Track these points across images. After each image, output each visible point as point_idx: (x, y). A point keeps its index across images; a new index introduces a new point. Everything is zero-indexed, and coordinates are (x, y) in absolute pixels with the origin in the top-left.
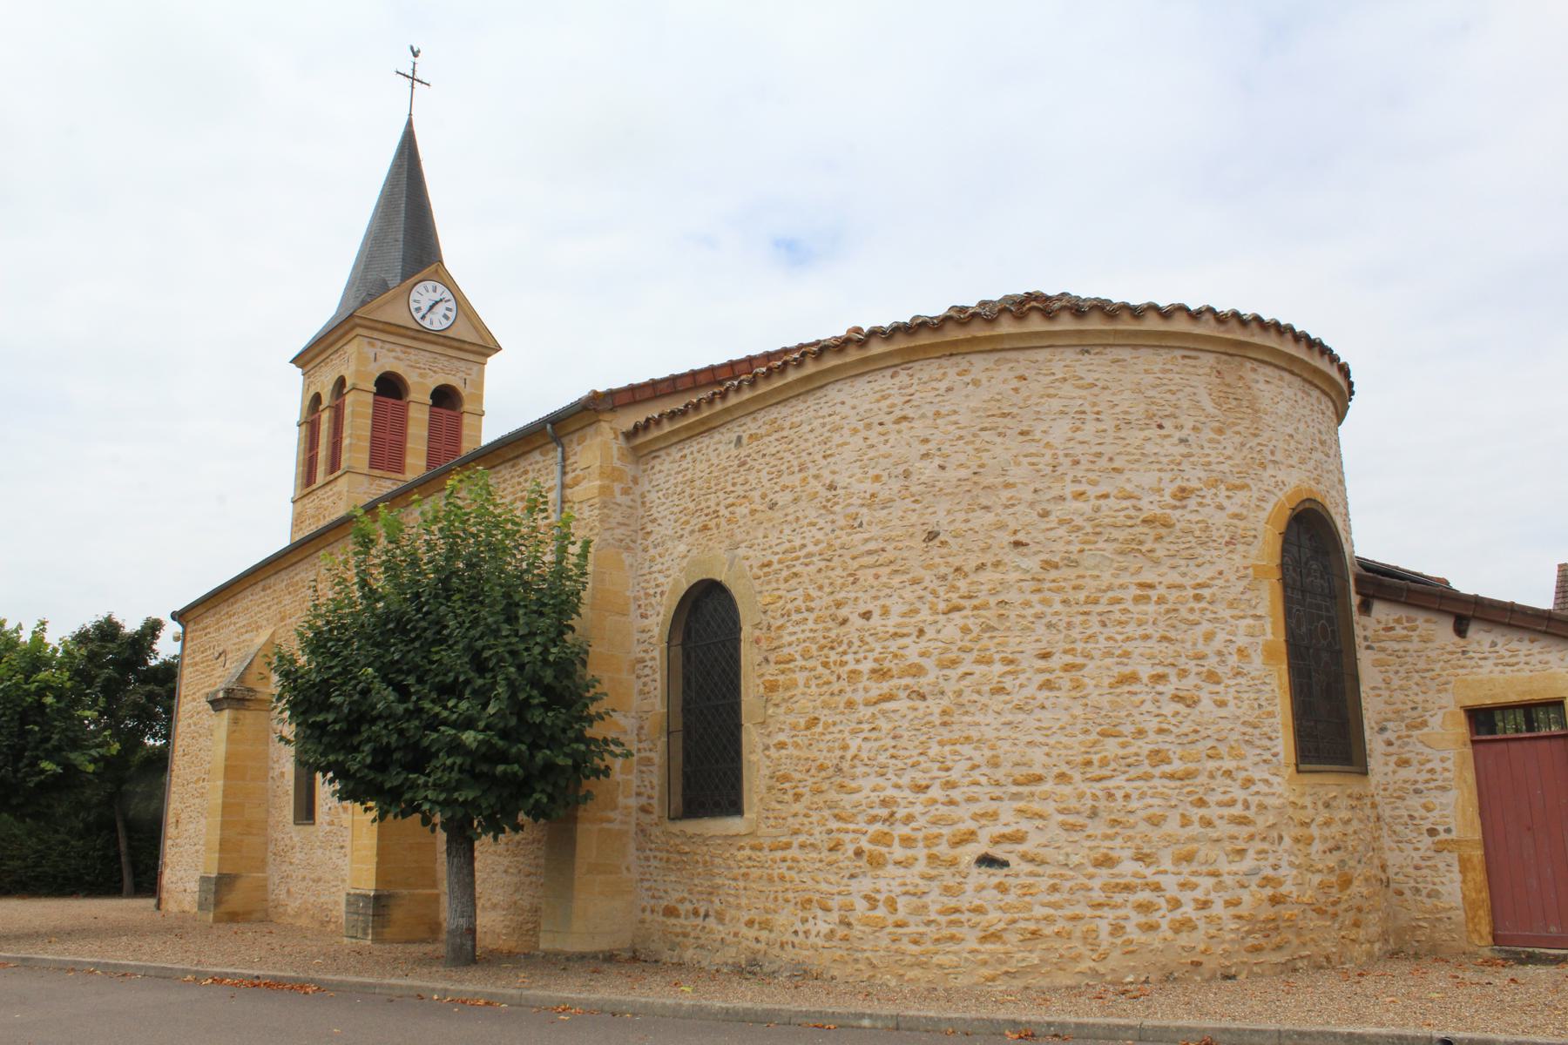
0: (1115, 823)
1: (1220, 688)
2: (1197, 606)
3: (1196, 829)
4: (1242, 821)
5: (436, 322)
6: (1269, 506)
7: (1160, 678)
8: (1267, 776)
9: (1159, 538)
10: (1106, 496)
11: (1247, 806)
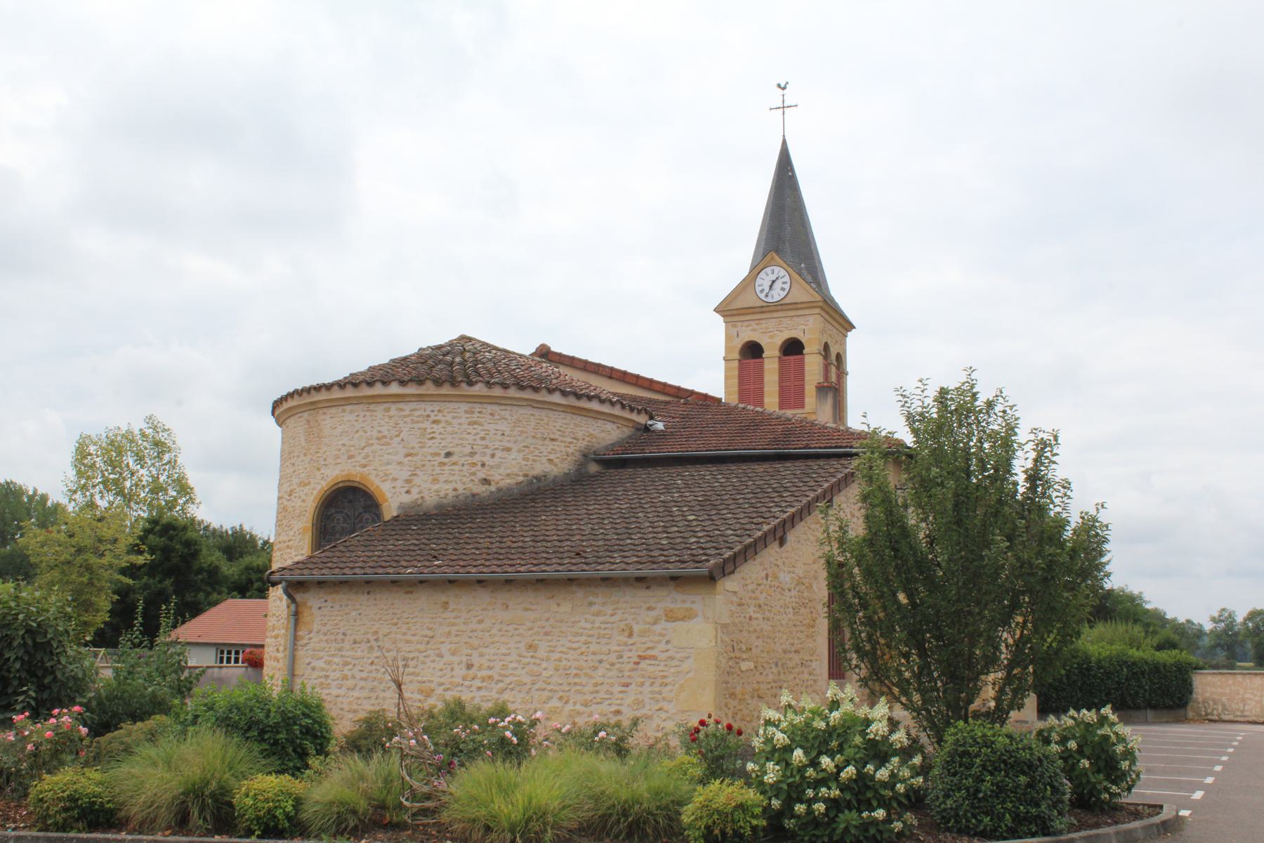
5: (777, 295)
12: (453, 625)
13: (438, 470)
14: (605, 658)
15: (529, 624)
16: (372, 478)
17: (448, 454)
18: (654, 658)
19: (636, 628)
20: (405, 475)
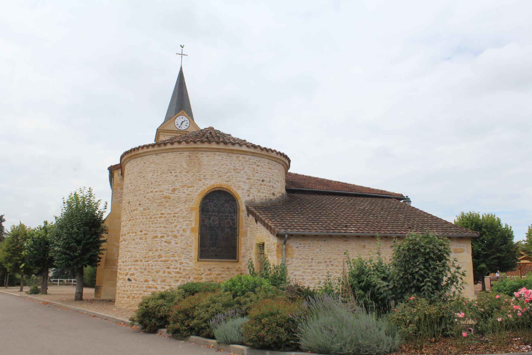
0: (149, 272)
1: (177, 239)
2: (174, 218)
3: (166, 274)
4: (178, 273)
6: (199, 191)
7: (162, 237)
8: (188, 262)
9: (167, 202)
10: (156, 192)
11: (180, 269)
13: (260, 186)
16: (232, 187)
17: (263, 181)
20: (247, 188)
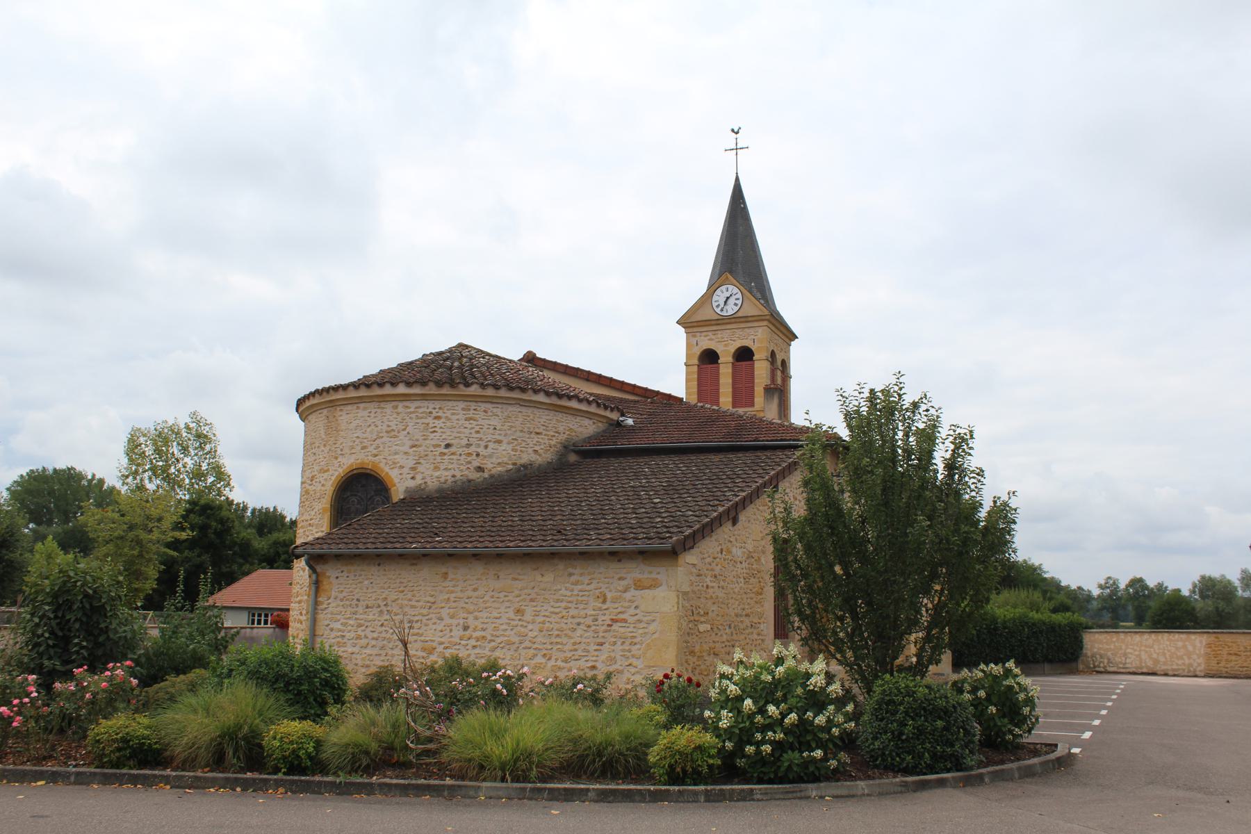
5: (731, 310)
12: (452, 592)
14: (582, 620)
15: (517, 592)
16: (382, 465)
17: (448, 446)
18: (625, 621)
19: (609, 595)
20: (411, 463)
